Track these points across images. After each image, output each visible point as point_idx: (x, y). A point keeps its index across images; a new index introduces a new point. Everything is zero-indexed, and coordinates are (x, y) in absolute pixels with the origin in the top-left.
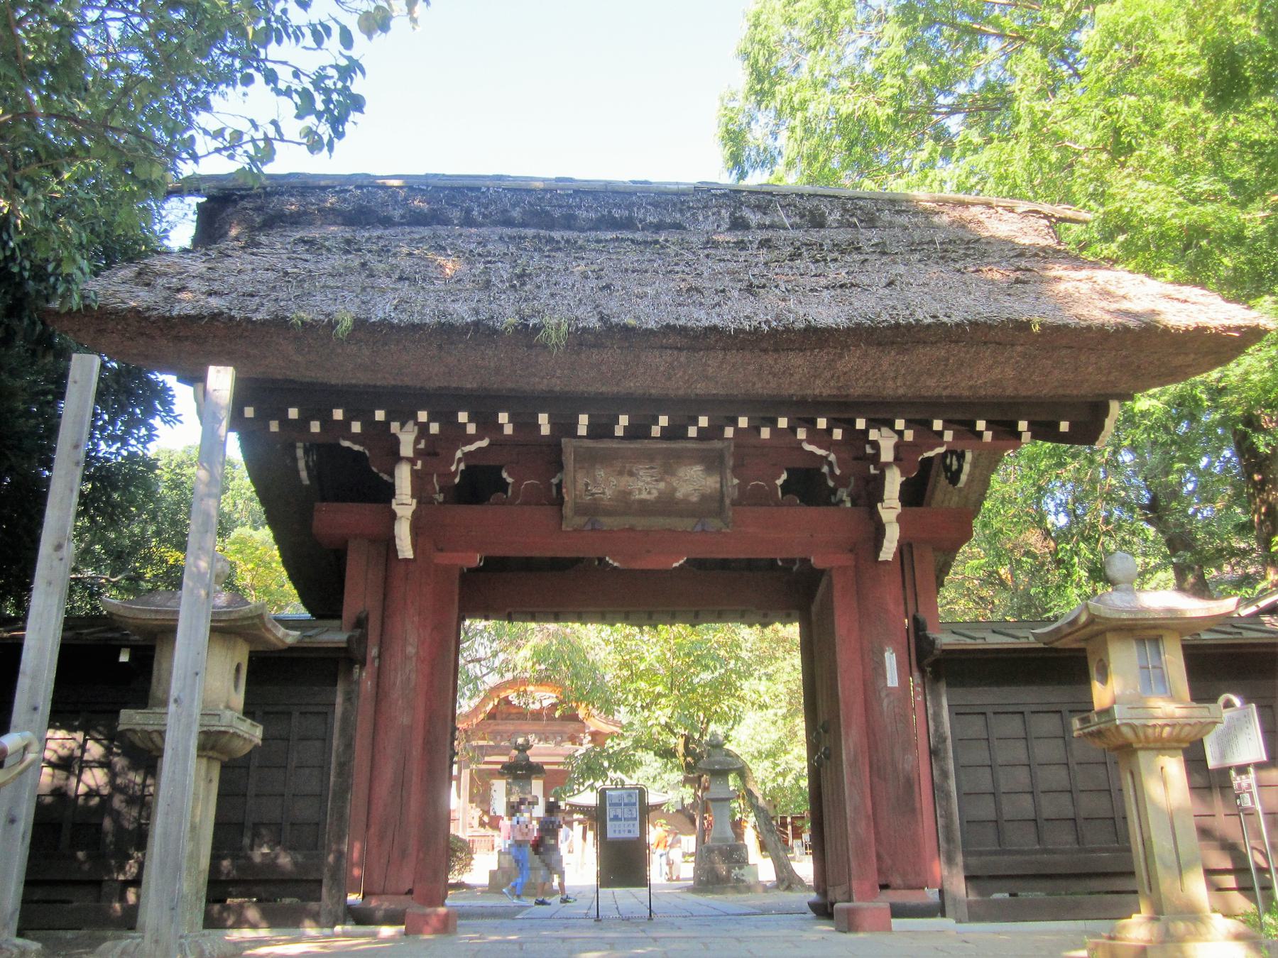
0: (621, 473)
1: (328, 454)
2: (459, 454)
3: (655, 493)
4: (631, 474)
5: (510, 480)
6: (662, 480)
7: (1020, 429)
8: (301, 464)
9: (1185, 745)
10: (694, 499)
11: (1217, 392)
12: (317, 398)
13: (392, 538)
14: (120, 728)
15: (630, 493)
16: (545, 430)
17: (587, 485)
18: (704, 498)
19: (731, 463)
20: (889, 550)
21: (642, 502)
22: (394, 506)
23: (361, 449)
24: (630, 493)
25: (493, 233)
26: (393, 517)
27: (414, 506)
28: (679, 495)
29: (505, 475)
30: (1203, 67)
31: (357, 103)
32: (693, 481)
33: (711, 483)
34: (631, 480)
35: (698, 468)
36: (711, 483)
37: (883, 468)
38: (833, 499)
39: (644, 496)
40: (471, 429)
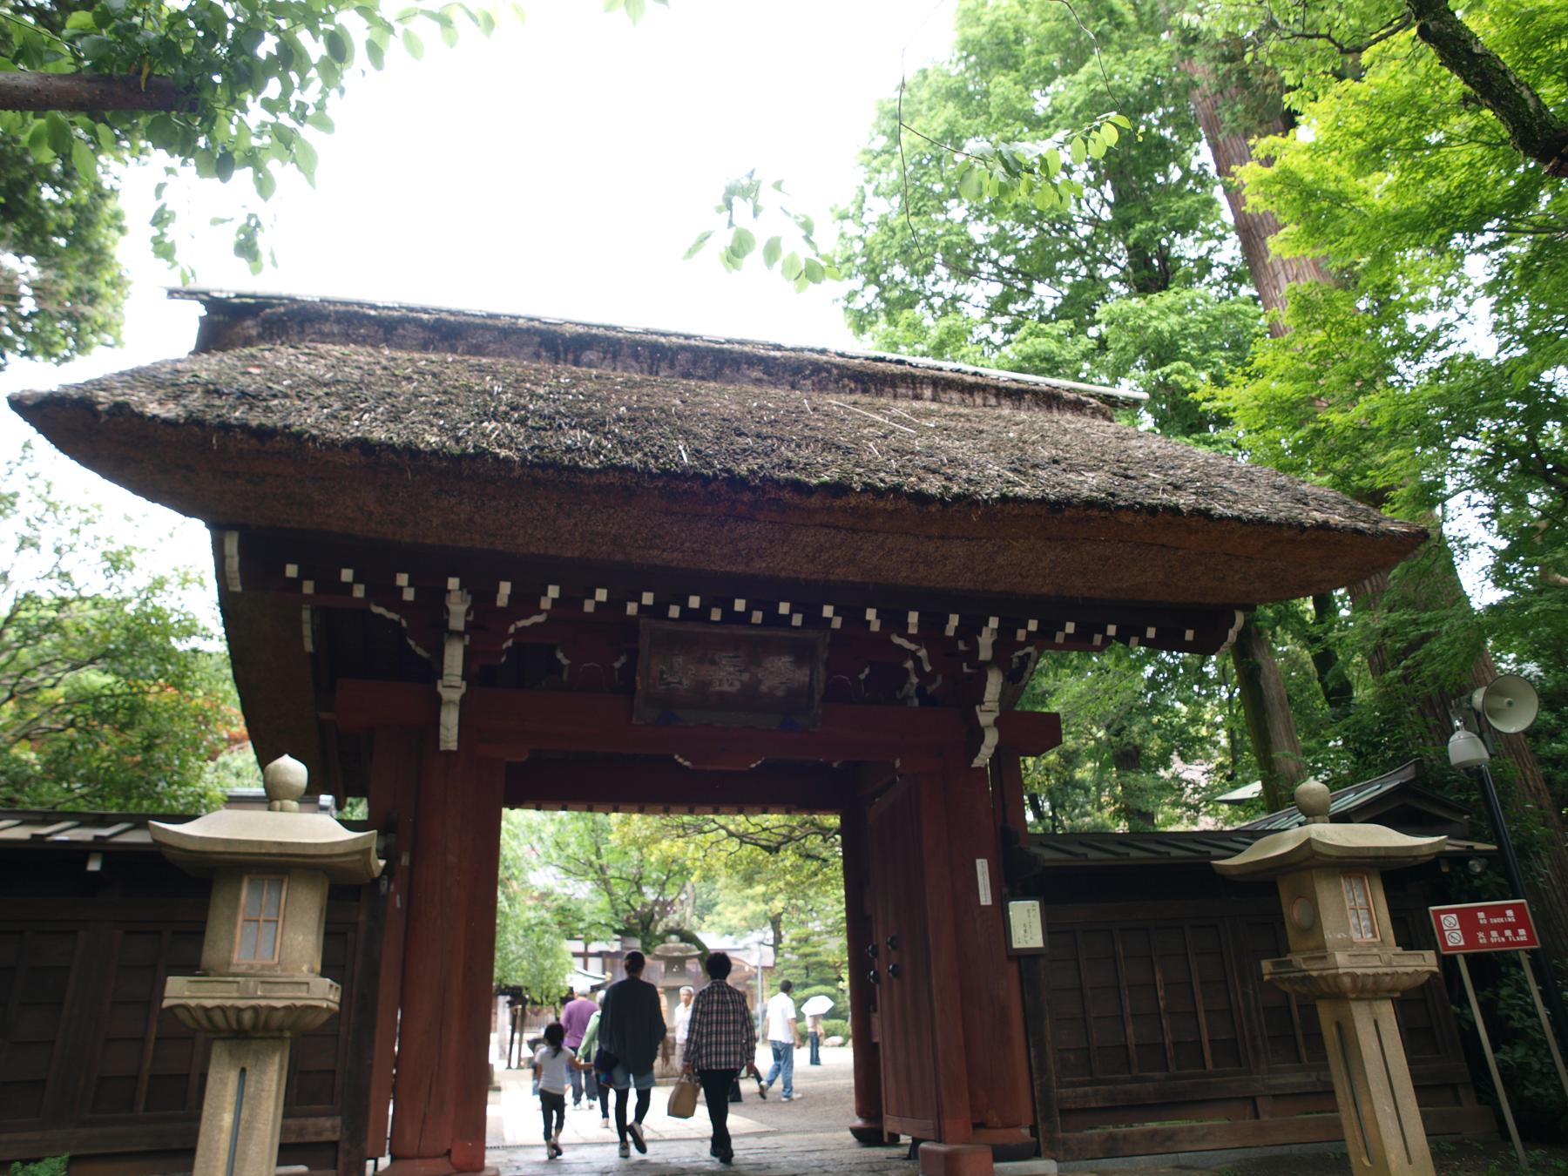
1: (338, 621)
2: (512, 629)
3: (738, 685)
4: (713, 662)
5: (565, 662)
6: (745, 671)
7: (450, 587)
8: (307, 630)
9: (1397, 995)
10: (780, 693)
12: (322, 553)
14: (166, 1003)
16: (875, 627)
17: (662, 672)
19: (825, 656)
20: (983, 758)
21: (722, 694)
22: (440, 689)
23: (396, 617)
26: (437, 703)
27: (464, 689)
28: (764, 688)
29: (560, 655)
30: (1524, 250)
31: (172, 245)
32: (780, 673)
33: (801, 676)
35: (786, 659)
36: (801, 676)
37: (982, 670)
38: (899, 696)
39: (726, 688)
40: (913, 630)
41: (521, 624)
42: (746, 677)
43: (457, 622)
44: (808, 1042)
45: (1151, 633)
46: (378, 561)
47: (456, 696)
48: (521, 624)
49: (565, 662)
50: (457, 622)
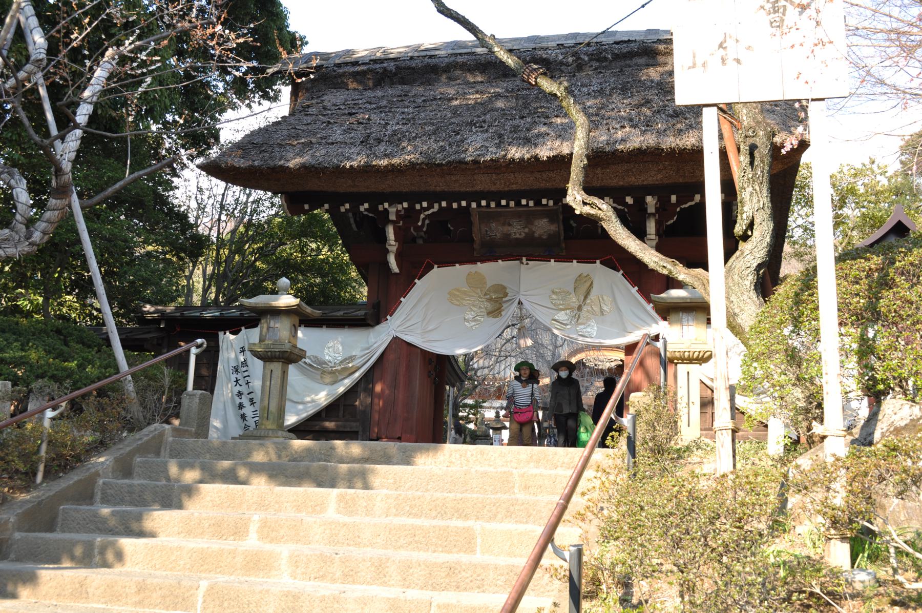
0: (504, 224)
3: (523, 235)
4: (510, 225)
5: (574, 225)
11: (313, 401)
13: (387, 263)
15: (510, 235)
18: (550, 236)
21: (517, 239)
24: (510, 235)
25: (495, 154)
26: (387, 251)
28: (536, 235)
33: (553, 228)
34: (509, 228)
35: (545, 220)
36: (553, 228)
39: (518, 236)
41: (683, 207)
42: (526, 230)
43: (651, 209)
44: (635, 601)
45: (306, 207)
46: (356, 199)
47: (394, 249)
48: (683, 207)
49: (574, 225)
50: (651, 209)
